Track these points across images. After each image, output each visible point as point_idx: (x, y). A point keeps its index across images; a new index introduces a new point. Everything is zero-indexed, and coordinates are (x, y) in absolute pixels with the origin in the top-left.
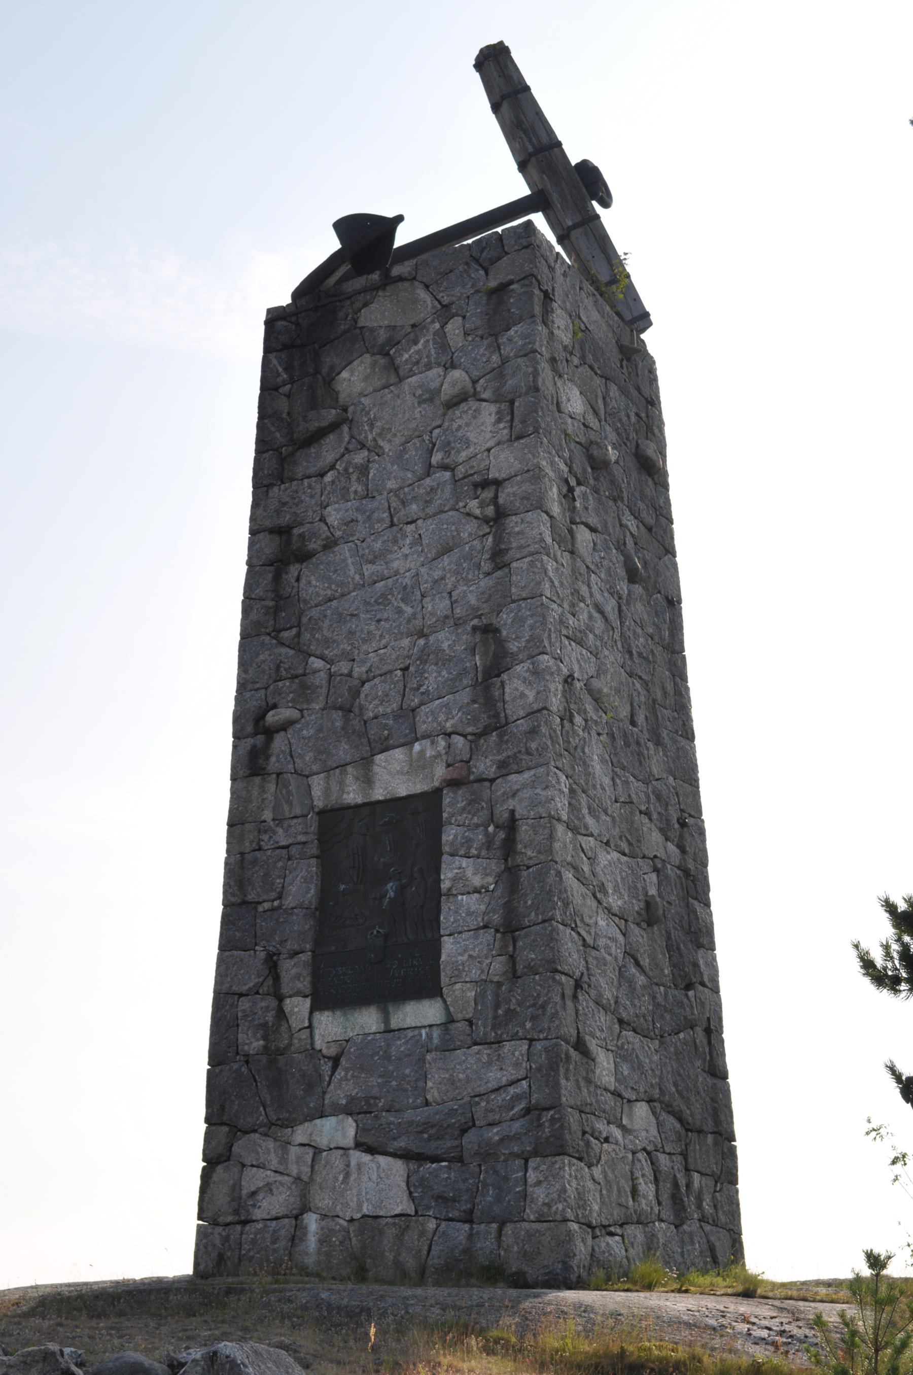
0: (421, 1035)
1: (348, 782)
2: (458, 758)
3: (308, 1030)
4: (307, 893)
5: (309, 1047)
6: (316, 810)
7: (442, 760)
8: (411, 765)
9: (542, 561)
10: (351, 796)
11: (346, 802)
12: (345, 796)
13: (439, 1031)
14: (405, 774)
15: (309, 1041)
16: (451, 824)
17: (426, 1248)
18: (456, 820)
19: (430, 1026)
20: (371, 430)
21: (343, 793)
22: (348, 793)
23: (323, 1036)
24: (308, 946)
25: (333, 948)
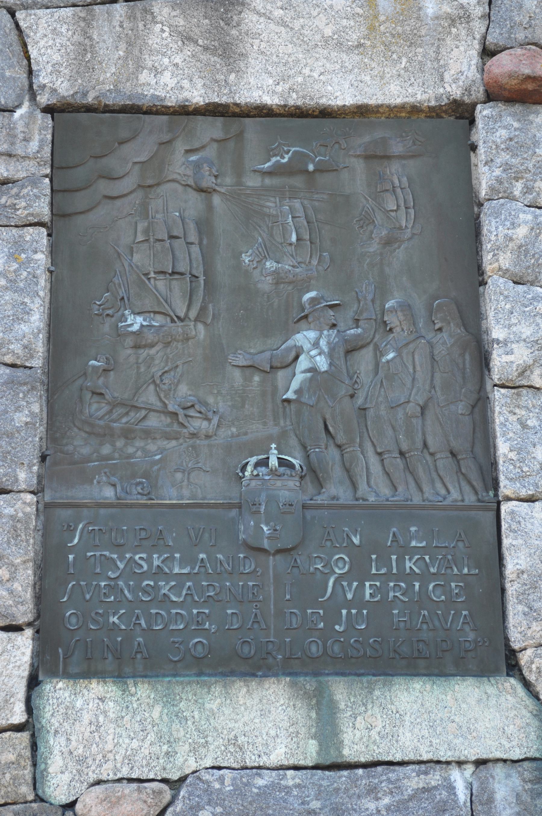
0: (451, 788)
1: (154, 41)
2: (521, 36)
3: (25, 736)
4: (18, 319)
5: (26, 791)
6: (44, 99)
7: (470, 32)
8: (372, 28)
9: (207, 39)
10: (167, 78)
11: (149, 92)
12: (145, 77)
13: (516, 781)
14: (350, 50)
15: (27, 773)
16: (511, 198)
17: (344, 511)
18: (528, 190)
19: (480, 763)
20: (299, 805)
21: (140, 67)
22: (156, 71)
23: (81, 761)
24: (22, 475)
25: (109, 493)
